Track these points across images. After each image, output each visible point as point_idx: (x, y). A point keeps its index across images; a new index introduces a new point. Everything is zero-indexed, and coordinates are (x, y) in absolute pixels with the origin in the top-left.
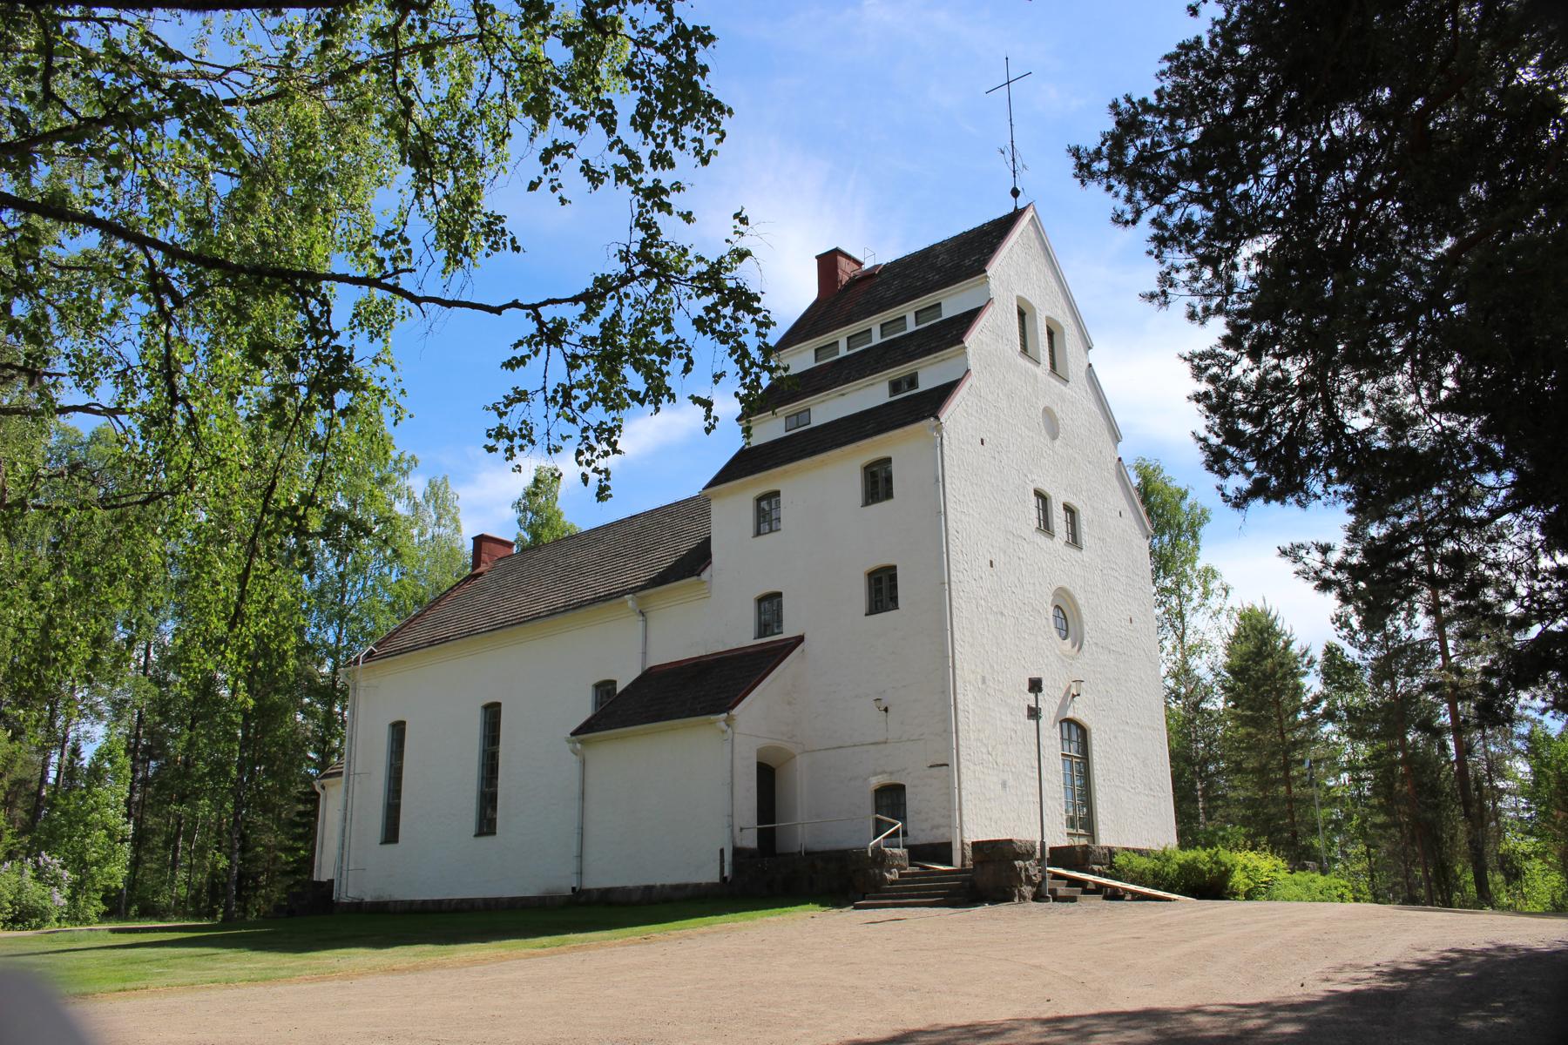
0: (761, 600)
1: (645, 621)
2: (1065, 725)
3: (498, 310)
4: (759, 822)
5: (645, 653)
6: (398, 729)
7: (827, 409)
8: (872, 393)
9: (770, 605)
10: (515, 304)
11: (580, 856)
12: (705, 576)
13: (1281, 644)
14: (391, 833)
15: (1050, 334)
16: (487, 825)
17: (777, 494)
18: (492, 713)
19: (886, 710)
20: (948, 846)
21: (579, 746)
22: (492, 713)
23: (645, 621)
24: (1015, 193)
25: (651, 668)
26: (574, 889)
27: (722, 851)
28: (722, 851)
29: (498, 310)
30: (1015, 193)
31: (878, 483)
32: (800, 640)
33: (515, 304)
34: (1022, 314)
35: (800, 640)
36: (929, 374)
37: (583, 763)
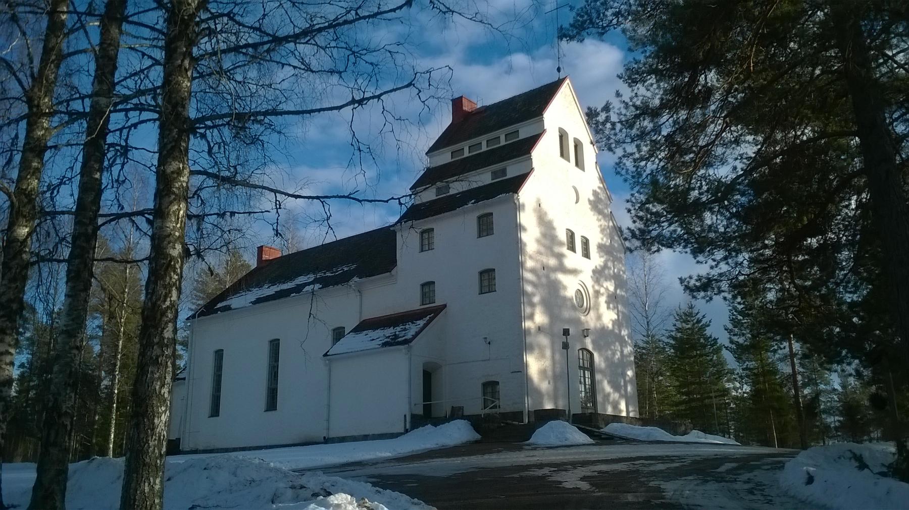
0: (423, 285)
1: (361, 295)
2: (581, 351)
3: (387, 201)
4: (424, 402)
5: (361, 313)
6: (219, 354)
7: (457, 187)
8: (483, 178)
9: (428, 287)
10: (393, 198)
11: (328, 420)
12: (393, 272)
13: (611, 306)
14: (215, 411)
15: (576, 147)
16: (272, 404)
17: (432, 230)
18: (275, 345)
19: (489, 343)
20: (521, 413)
21: (327, 362)
22: (275, 345)
23: (361, 295)
24: (559, 70)
25: (364, 320)
26: (325, 437)
27: (405, 416)
28: (405, 416)
29: (387, 201)
30: (559, 70)
31: (485, 226)
32: (445, 306)
33: (393, 198)
34: (561, 137)
35: (445, 306)
36: (512, 171)
37: (330, 370)
